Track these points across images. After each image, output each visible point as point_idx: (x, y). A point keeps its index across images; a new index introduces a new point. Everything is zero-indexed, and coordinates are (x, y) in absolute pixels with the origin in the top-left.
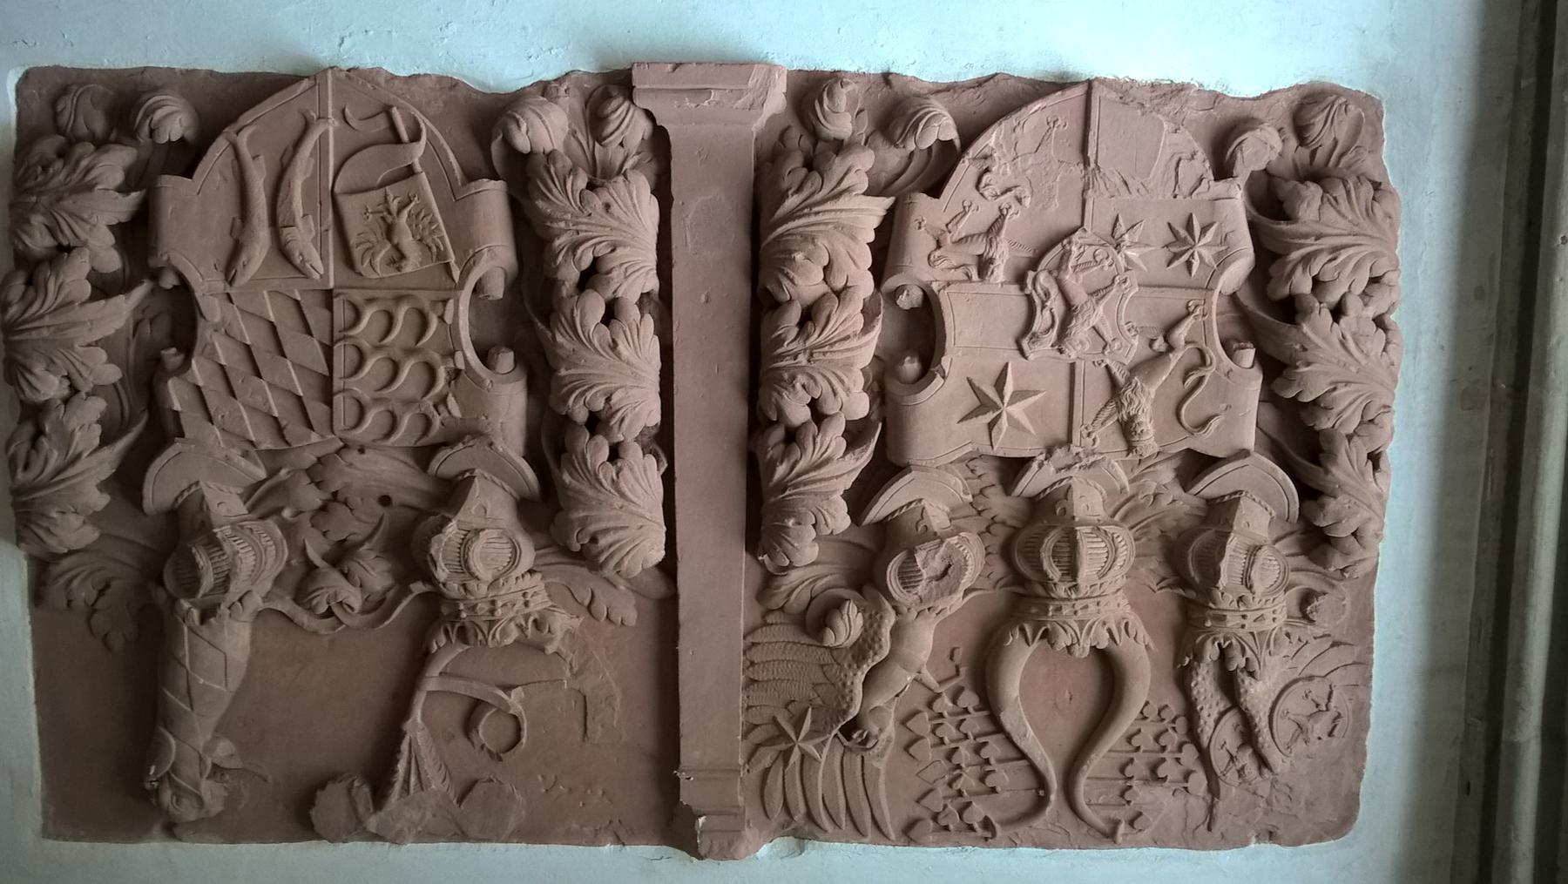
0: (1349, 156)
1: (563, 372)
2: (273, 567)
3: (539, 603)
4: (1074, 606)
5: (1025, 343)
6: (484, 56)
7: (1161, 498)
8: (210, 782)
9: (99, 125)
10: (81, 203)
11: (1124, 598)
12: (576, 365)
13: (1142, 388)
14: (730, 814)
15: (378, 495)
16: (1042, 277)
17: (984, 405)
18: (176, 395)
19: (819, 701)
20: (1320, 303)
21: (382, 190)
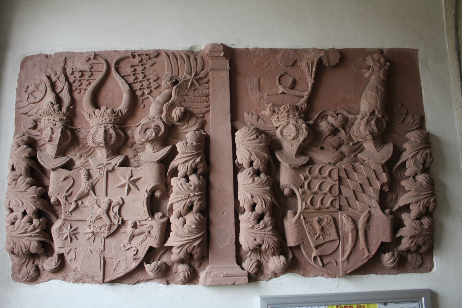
0: (22, 262)
1: (268, 188)
2: (354, 128)
3: (274, 118)
4: (106, 121)
5: (121, 202)
6: (295, 284)
7: (79, 156)
8: (370, 65)
9: (409, 257)
10: (413, 233)
11: (91, 125)
12: (264, 190)
13: (85, 189)
14: (213, 57)
15: (324, 150)
16: (116, 222)
17: (134, 182)
18: (384, 177)
19: (186, 90)
20: (30, 216)
21: (325, 241)
